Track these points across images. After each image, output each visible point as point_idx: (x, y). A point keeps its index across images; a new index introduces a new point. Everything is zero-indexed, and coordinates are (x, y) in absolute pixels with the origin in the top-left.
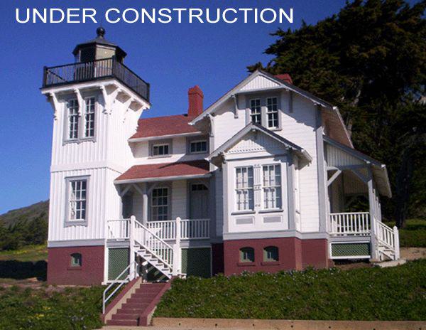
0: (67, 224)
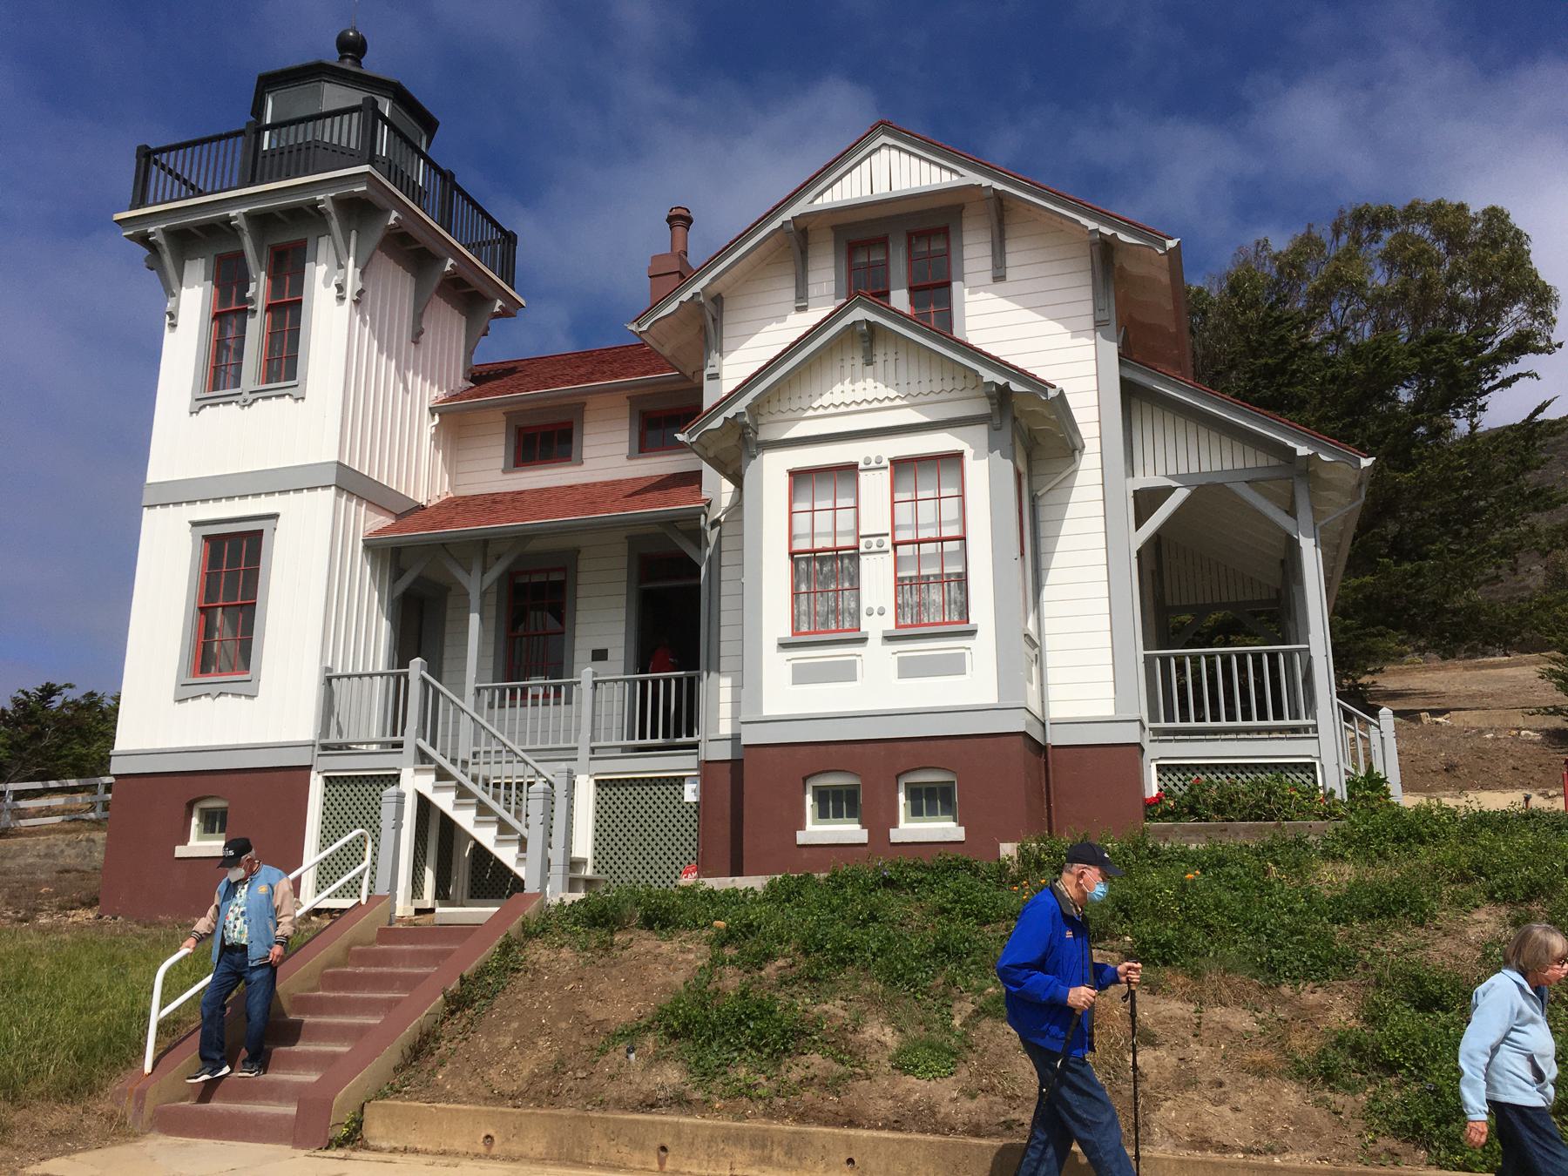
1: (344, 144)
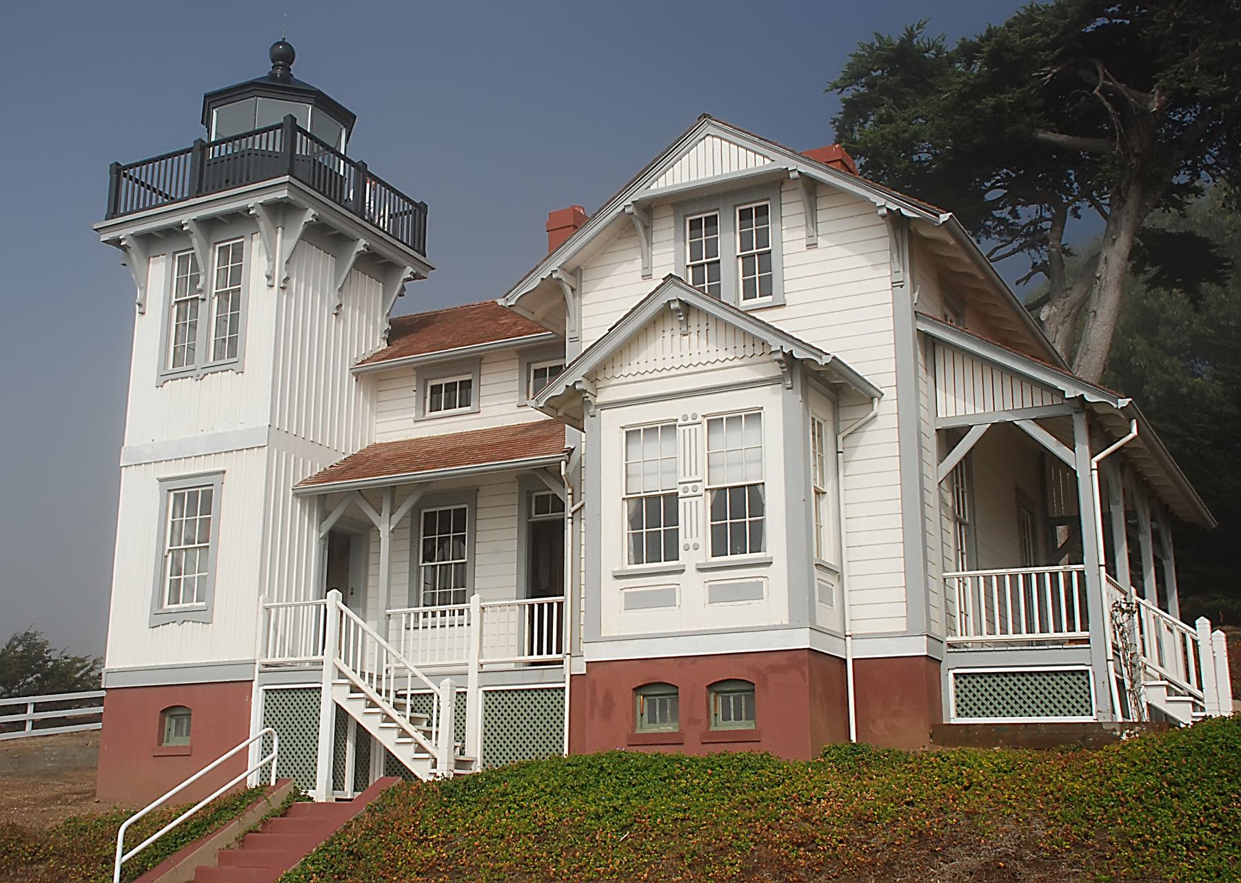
0: (159, 619)
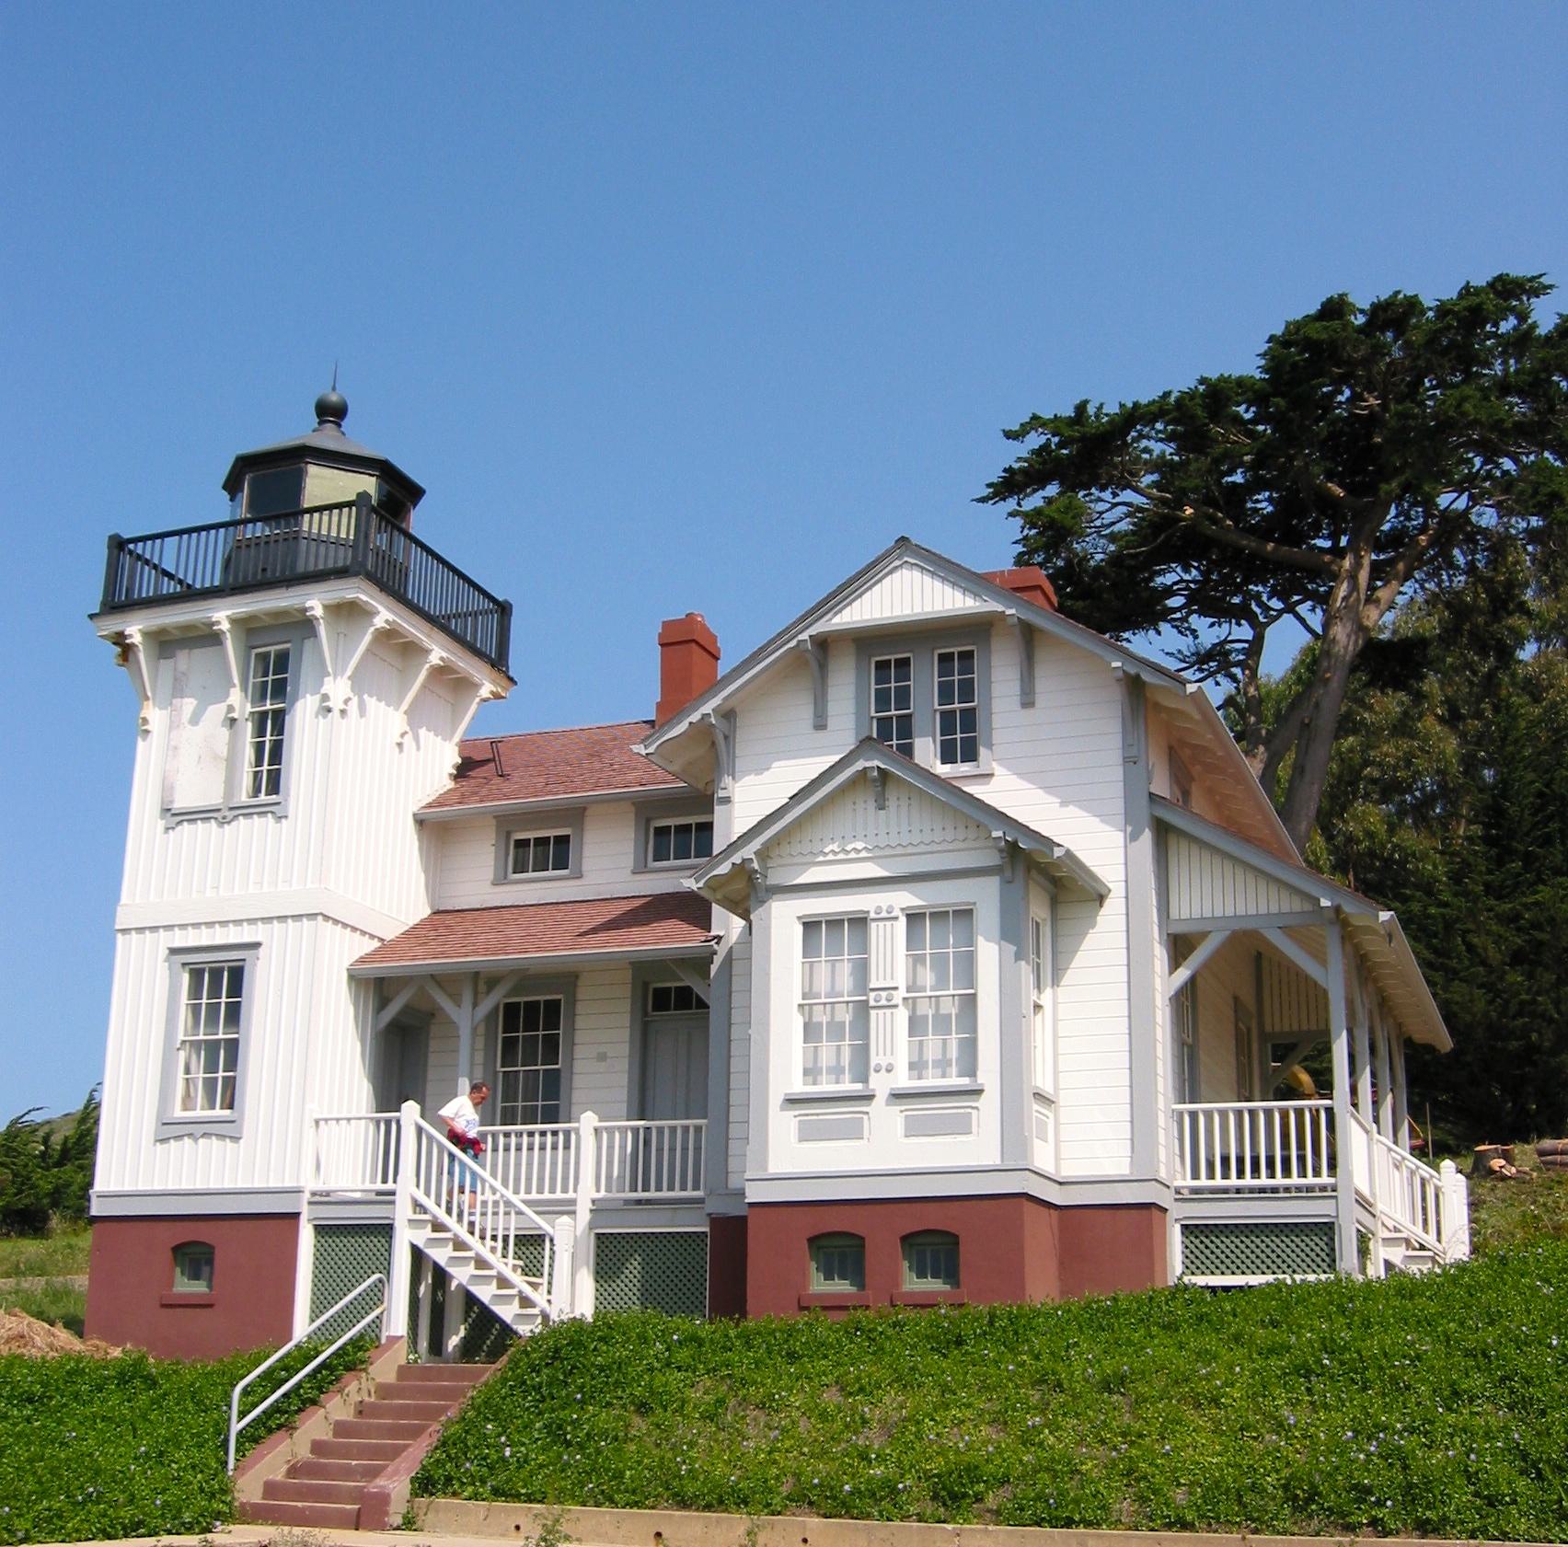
0: (169, 1131)
1: (324, 532)
